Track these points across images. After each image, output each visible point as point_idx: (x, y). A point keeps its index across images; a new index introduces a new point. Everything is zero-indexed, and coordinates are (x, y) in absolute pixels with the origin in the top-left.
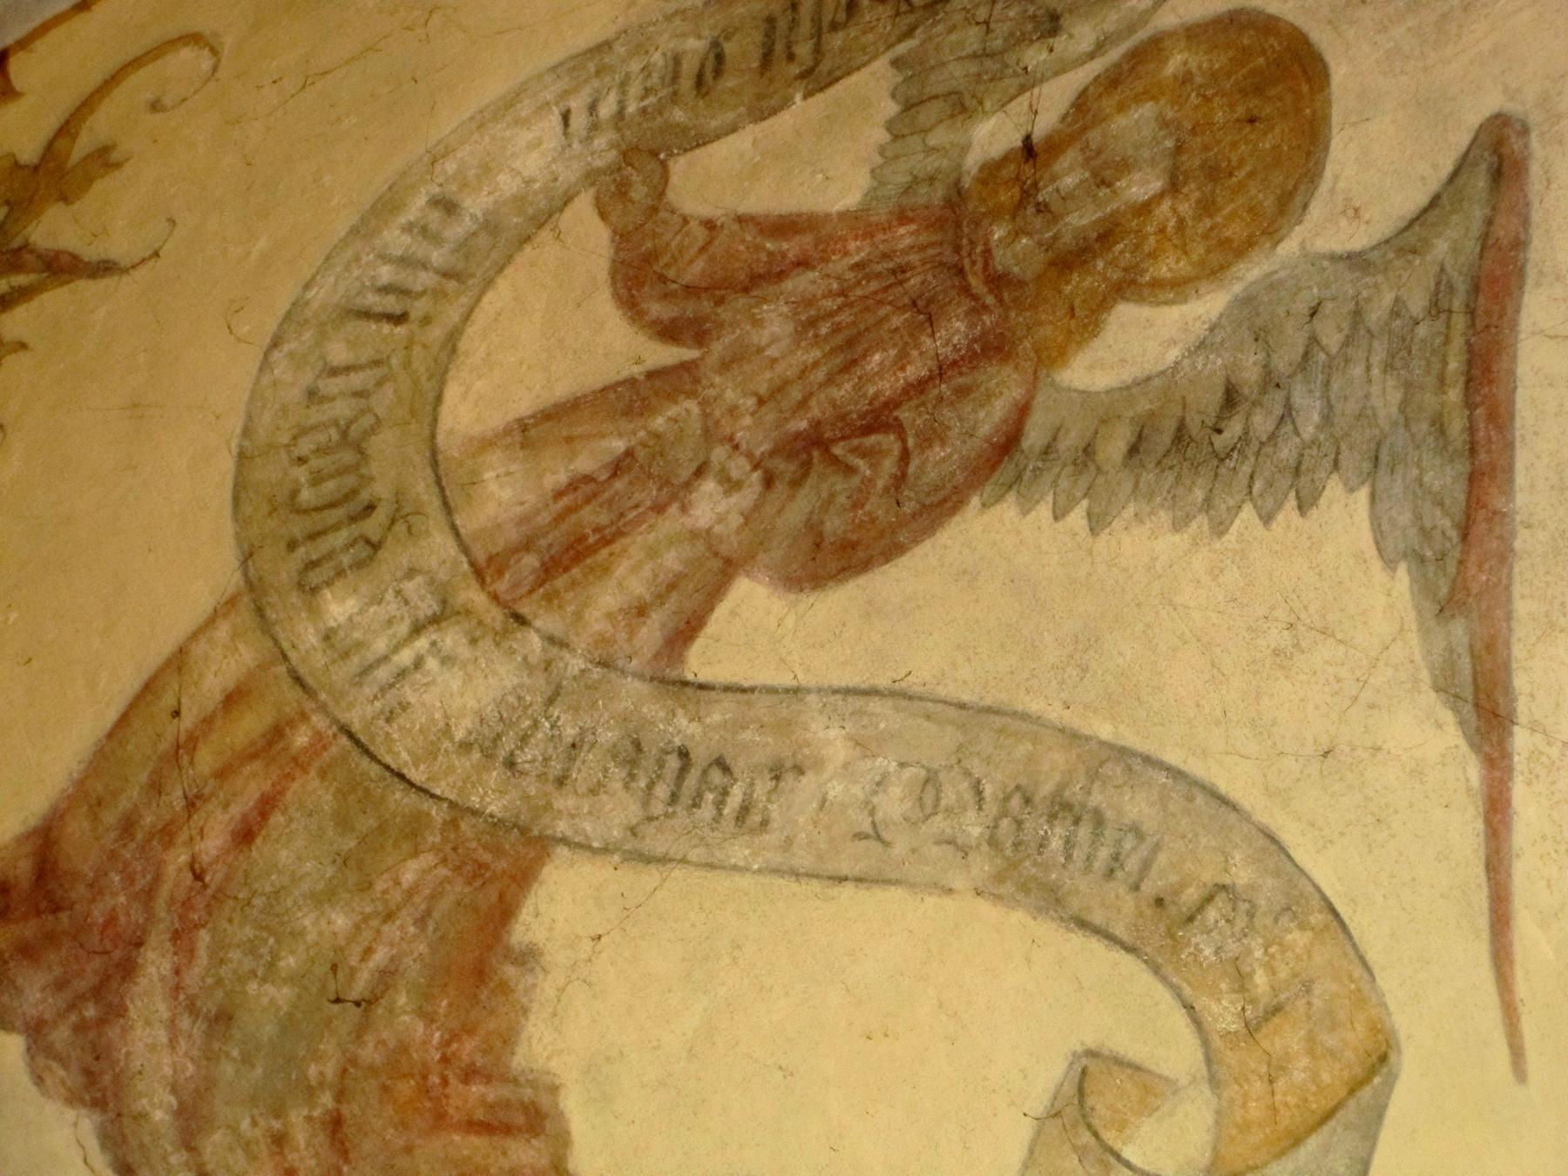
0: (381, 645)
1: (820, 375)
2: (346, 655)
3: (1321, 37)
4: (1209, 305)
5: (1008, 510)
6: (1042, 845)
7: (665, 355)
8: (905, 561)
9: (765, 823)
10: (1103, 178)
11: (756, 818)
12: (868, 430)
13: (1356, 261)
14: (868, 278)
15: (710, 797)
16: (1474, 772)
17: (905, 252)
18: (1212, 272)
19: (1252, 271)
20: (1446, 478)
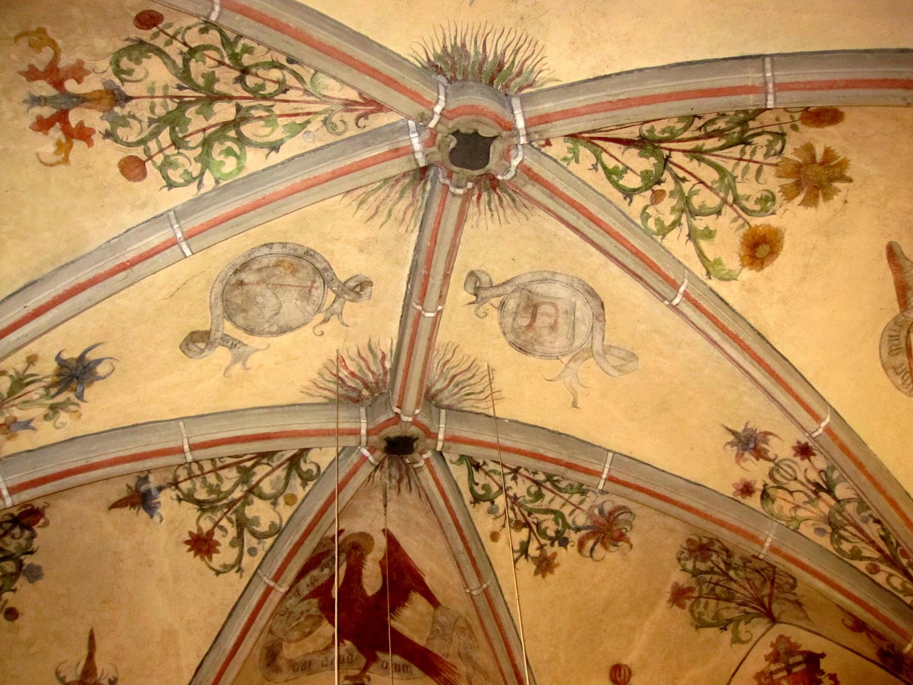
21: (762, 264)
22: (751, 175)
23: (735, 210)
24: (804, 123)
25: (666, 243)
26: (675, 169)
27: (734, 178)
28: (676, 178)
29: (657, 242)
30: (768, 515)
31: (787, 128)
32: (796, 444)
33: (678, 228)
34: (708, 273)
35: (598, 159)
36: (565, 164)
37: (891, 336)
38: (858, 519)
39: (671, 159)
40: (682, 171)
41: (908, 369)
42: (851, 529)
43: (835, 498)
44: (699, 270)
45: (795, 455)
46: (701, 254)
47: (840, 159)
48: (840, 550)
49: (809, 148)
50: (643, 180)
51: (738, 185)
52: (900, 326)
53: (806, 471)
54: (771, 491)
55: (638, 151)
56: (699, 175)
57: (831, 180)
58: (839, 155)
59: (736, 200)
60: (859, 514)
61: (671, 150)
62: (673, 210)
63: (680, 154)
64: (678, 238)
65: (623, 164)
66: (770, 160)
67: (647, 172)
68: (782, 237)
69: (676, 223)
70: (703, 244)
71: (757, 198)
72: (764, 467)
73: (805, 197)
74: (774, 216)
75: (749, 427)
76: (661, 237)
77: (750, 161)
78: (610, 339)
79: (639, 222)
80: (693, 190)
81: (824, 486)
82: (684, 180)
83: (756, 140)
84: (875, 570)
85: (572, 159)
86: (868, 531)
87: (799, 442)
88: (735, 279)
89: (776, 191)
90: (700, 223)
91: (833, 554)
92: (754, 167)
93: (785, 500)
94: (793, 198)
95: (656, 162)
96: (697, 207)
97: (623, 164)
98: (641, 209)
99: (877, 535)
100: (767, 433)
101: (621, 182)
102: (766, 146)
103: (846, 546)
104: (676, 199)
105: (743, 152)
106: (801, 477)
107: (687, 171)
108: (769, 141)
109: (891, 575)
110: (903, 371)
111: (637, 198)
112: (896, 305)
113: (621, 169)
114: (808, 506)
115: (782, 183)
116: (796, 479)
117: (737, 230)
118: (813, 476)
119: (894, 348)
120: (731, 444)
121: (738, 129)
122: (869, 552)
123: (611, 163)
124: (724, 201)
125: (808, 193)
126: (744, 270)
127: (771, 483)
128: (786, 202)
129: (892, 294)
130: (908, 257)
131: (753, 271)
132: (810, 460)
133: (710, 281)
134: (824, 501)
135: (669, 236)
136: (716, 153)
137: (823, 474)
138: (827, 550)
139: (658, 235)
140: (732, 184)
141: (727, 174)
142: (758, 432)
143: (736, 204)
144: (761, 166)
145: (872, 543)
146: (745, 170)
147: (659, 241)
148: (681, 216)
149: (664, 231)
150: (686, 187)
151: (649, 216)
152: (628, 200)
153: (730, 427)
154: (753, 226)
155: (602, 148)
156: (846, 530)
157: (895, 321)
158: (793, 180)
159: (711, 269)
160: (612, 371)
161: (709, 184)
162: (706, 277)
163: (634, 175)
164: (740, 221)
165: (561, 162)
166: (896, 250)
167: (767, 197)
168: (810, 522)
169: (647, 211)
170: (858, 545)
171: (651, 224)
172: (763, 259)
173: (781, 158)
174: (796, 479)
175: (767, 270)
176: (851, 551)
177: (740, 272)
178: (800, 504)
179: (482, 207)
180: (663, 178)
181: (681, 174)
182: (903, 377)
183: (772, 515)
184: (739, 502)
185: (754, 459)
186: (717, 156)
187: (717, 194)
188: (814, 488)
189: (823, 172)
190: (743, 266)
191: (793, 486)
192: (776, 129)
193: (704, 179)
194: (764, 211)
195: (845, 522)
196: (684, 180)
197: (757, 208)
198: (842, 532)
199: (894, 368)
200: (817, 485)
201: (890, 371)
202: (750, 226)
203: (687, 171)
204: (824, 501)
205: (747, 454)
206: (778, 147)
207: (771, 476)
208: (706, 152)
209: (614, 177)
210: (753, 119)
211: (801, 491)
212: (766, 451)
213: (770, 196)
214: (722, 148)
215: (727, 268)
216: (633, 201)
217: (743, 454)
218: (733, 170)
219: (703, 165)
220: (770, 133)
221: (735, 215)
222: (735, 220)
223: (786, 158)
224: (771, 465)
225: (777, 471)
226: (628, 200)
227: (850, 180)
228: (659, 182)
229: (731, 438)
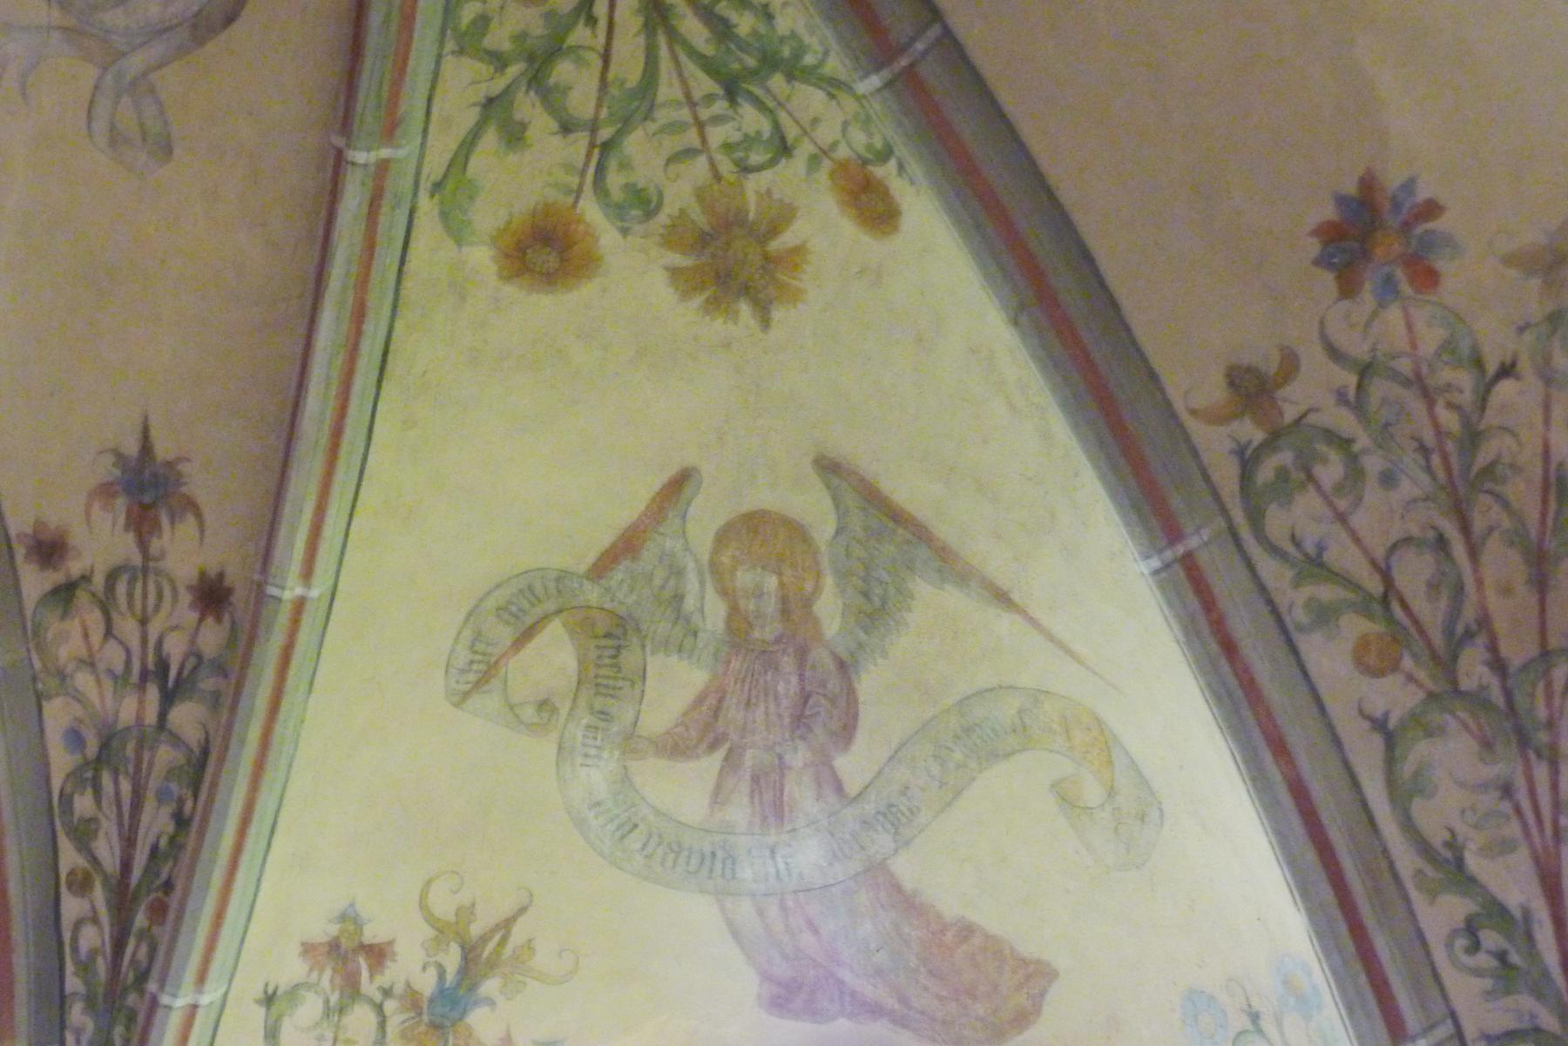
0: (772, 870)
1: (772, 706)
2: (767, 879)
3: (746, 507)
4: (829, 581)
5: (864, 676)
6: (975, 745)
7: (720, 754)
8: (861, 715)
9: (918, 807)
10: (759, 594)
11: (915, 809)
12: (806, 702)
13: (839, 531)
14: (743, 681)
15: (899, 815)
16: (1018, 618)
17: (742, 666)
18: (819, 575)
19: (825, 562)
20: (923, 552)
22: (672, 144)
23: (589, 156)
24: (832, 174)
25: (449, 62)
29: (442, 43)
30: (29, 625)
31: (805, 149)
32: (212, 572)
34: (437, 186)
37: (530, 588)
38: (153, 784)
41: (493, 660)
42: (126, 787)
43: (162, 716)
44: (435, 164)
45: (190, 588)
47: (794, 282)
48: (66, 801)
49: (781, 218)
52: (559, 591)
53: (176, 628)
54: (82, 597)
56: (617, 44)
57: (746, 290)
59: (607, 147)
60: (166, 778)
70: (490, 138)
71: (634, 185)
72: (124, 547)
75: (180, 467)
77: (701, 126)
78: (171, 80)
81: (171, 684)
82: (592, 21)
84: (81, 885)
86: (145, 818)
87: (221, 576)
89: (669, 210)
90: (528, 107)
91: (50, 793)
92: (692, 137)
93: (86, 636)
96: (552, 81)
99: (151, 839)
100: (192, 506)
102: (746, 136)
103: (84, 804)
105: (710, 98)
106: (154, 629)
108: (758, 133)
109: (95, 920)
110: (484, 654)
112: (591, 557)
114: (108, 684)
116: (144, 622)
118: (175, 648)
119: (514, 609)
120: (119, 456)
121: (751, 62)
122: (107, 850)
124: (594, 127)
127: (99, 581)
129: (605, 538)
130: (689, 517)
132: (201, 620)
134: (141, 702)
136: (683, 58)
137: (192, 661)
138: (47, 780)
142: (184, 489)
145: (129, 842)
146: (674, 127)
149: (470, 41)
153: (154, 433)
154: (578, 211)
156: (116, 782)
157: (562, 576)
158: (707, 228)
159: (450, 186)
160: (100, 126)
161: (611, 75)
162: (429, 185)
166: (688, 490)
167: (649, 202)
168: (78, 710)
170: (105, 824)
174: (144, 622)
175: (511, 291)
176: (82, 820)
178: (101, 667)
182: (472, 662)
183: (36, 633)
184: (12, 557)
185: (122, 520)
188: (151, 666)
191: (128, 627)
192: (792, 132)
194: (617, 212)
195: (131, 769)
196: (592, 21)
197: (617, 195)
198: (106, 780)
199: (478, 636)
200: (163, 665)
201: (467, 634)
204: (141, 702)
205: (121, 502)
207: (112, 577)
208: (673, 35)
210: (790, 77)
211: (128, 651)
212: (156, 527)
213: (653, 206)
214: (693, 53)
217: (114, 495)
218: (664, 105)
219: (641, 40)
220: (777, 127)
221: (579, 161)
224: (137, 560)
225: (131, 582)
227: (766, 323)
229: (132, 448)
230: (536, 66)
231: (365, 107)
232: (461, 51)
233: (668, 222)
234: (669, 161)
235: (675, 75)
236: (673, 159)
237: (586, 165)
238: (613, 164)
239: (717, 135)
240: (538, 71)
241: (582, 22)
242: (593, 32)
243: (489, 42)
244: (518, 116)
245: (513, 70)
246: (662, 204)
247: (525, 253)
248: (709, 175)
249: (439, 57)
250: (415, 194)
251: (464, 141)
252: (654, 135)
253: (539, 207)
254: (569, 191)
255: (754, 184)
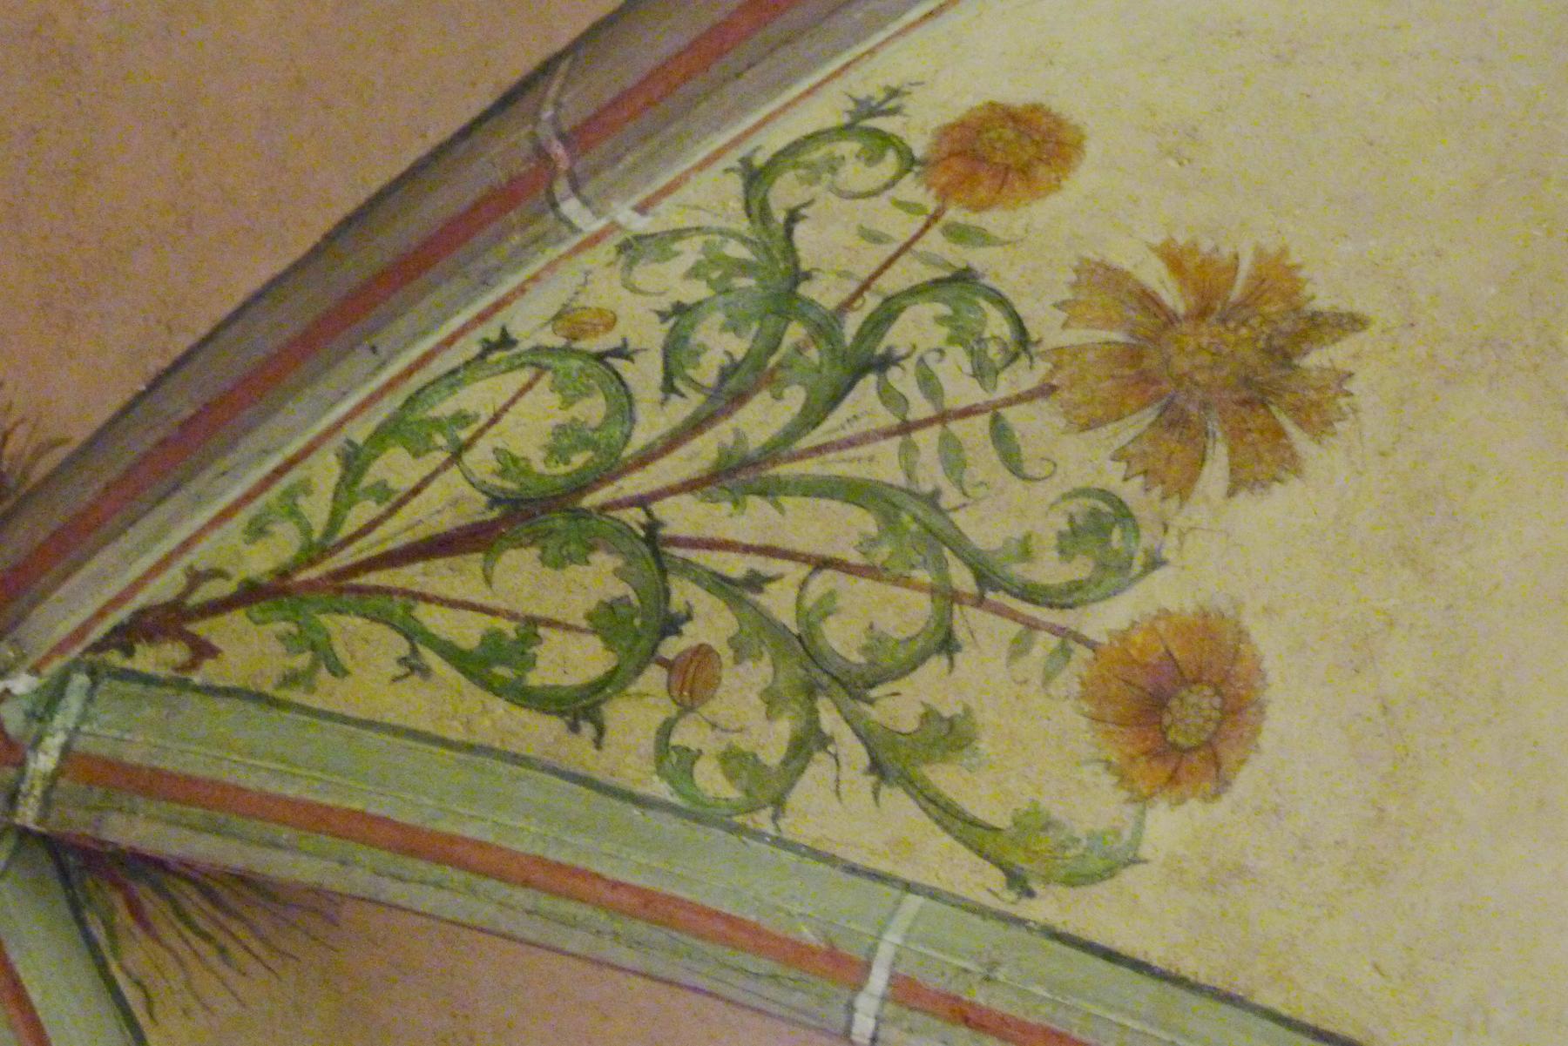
21: (1218, 766)
22: (984, 461)
23: (1000, 611)
25: (796, 826)
26: (697, 556)
27: (933, 499)
28: (720, 584)
29: (758, 835)
33: (818, 756)
34: (1017, 881)
35: (413, 634)
36: (296, 695)
39: (664, 532)
40: (732, 556)
46: (946, 814)
50: (609, 643)
51: (959, 518)
55: (535, 551)
57: (1283, 355)
58: (1226, 251)
61: (642, 502)
62: (771, 699)
63: (686, 499)
64: (838, 793)
65: (513, 616)
66: (1005, 386)
67: (610, 607)
68: (1241, 634)
69: (808, 743)
70: (944, 777)
71: (1061, 535)
73: (1233, 452)
74: (1158, 575)
76: (770, 810)
79: (659, 788)
80: (808, 603)
82: (756, 582)
83: (896, 337)
85: (314, 666)
88: (1135, 861)
94: (1193, 479)
95: (620, 562)
96: (856, 658)
97: (513, 616)
98: (648, 745)
101: (534, 679)
102: (951, 341)
104: (767, 659)
107: (748, 549)
111: (617, 712)
113: (512, 635)
115: (1117, 445)
117: (1048, 679)
123: (467, 631)
124: (948, 597)
125: (1236, 435)
126: (1151, 815)
128: (1173, 503)
131: (1194, 804)
133: (1034, 903)
135: (795, 799)
136: (804, 443)
139: (752, 809)
140: (936, 522)
141: (899, 499)
143: (995, 589)
144: (996, 418)
147: (769, 828)
148: (814, 711)
150: (779, 602)
151: (690, 757)
152: (588, 729)
154: (1104, 639)
155: (405, 593)
158: (1150, 415)
159: (1017, 858)
161: (854, 558)
162: (1010, 896)
163: (570, 637)
164: (1045, 643)
165: (283, 694)
167: (1094, 513)
169: (675, 740)
171: (711, 780)
172: (1209, 743)
173: (1044, 355)
175: (1247, 781)
177: (1140, 824)
179: (170, 937)
180: (677, 604)
181: (735, 566)
186: (819, 450)
187: (903, 581)
189: (1231, 338)
190: (1143, 800)
193: (829, 552)
196: (756, 582)
202: (1092, 645)
203: (748, 549)
206: (997, 325)
208: (774, 452)
209: (501, 671)
213: (1104, 507)
214: (811, 417)
215: (1079, 832)
216: (608, 724)
219: (787, 502)
222: (1019, 649)
223: (1059, 350)
226: (588, 729)
228: (672, 625)
230: (825, 679)
231: (187, 942)
232: (779, 804)
233: (1138, 482)
234: (1016, 470)
235: (851, 452)
236: (1012, 460)
237: (1014, 616)
238: (1019, 571)
239: (971, 393)
240: (835, 678)
241: (763, 600)
242: (770, 580)
243: (773, 755)
244: (910, 724)
245: (829, 719)
246: (1102, 491)
247: (1174, 746)
248: (1041, 403)
249: (779, 842)
250: (1020, 922)
251: (938, 822)
252: (965, 494)
253: (1086, 709)
254: (1065, 652)
255: (1047, 327)
